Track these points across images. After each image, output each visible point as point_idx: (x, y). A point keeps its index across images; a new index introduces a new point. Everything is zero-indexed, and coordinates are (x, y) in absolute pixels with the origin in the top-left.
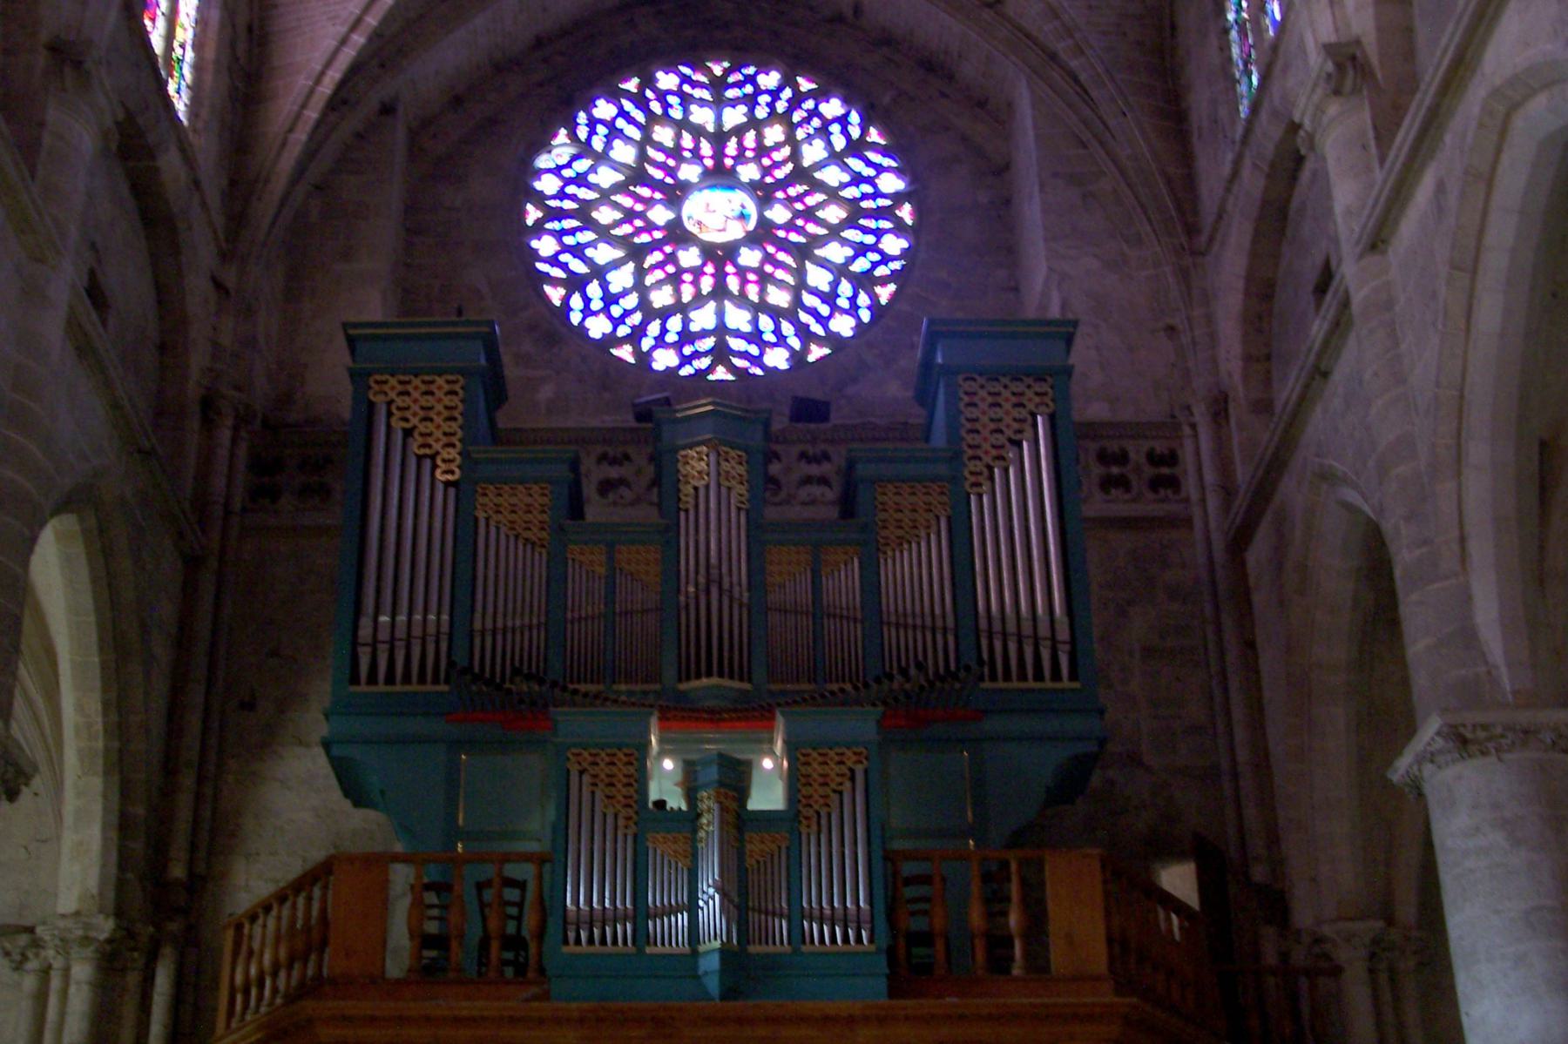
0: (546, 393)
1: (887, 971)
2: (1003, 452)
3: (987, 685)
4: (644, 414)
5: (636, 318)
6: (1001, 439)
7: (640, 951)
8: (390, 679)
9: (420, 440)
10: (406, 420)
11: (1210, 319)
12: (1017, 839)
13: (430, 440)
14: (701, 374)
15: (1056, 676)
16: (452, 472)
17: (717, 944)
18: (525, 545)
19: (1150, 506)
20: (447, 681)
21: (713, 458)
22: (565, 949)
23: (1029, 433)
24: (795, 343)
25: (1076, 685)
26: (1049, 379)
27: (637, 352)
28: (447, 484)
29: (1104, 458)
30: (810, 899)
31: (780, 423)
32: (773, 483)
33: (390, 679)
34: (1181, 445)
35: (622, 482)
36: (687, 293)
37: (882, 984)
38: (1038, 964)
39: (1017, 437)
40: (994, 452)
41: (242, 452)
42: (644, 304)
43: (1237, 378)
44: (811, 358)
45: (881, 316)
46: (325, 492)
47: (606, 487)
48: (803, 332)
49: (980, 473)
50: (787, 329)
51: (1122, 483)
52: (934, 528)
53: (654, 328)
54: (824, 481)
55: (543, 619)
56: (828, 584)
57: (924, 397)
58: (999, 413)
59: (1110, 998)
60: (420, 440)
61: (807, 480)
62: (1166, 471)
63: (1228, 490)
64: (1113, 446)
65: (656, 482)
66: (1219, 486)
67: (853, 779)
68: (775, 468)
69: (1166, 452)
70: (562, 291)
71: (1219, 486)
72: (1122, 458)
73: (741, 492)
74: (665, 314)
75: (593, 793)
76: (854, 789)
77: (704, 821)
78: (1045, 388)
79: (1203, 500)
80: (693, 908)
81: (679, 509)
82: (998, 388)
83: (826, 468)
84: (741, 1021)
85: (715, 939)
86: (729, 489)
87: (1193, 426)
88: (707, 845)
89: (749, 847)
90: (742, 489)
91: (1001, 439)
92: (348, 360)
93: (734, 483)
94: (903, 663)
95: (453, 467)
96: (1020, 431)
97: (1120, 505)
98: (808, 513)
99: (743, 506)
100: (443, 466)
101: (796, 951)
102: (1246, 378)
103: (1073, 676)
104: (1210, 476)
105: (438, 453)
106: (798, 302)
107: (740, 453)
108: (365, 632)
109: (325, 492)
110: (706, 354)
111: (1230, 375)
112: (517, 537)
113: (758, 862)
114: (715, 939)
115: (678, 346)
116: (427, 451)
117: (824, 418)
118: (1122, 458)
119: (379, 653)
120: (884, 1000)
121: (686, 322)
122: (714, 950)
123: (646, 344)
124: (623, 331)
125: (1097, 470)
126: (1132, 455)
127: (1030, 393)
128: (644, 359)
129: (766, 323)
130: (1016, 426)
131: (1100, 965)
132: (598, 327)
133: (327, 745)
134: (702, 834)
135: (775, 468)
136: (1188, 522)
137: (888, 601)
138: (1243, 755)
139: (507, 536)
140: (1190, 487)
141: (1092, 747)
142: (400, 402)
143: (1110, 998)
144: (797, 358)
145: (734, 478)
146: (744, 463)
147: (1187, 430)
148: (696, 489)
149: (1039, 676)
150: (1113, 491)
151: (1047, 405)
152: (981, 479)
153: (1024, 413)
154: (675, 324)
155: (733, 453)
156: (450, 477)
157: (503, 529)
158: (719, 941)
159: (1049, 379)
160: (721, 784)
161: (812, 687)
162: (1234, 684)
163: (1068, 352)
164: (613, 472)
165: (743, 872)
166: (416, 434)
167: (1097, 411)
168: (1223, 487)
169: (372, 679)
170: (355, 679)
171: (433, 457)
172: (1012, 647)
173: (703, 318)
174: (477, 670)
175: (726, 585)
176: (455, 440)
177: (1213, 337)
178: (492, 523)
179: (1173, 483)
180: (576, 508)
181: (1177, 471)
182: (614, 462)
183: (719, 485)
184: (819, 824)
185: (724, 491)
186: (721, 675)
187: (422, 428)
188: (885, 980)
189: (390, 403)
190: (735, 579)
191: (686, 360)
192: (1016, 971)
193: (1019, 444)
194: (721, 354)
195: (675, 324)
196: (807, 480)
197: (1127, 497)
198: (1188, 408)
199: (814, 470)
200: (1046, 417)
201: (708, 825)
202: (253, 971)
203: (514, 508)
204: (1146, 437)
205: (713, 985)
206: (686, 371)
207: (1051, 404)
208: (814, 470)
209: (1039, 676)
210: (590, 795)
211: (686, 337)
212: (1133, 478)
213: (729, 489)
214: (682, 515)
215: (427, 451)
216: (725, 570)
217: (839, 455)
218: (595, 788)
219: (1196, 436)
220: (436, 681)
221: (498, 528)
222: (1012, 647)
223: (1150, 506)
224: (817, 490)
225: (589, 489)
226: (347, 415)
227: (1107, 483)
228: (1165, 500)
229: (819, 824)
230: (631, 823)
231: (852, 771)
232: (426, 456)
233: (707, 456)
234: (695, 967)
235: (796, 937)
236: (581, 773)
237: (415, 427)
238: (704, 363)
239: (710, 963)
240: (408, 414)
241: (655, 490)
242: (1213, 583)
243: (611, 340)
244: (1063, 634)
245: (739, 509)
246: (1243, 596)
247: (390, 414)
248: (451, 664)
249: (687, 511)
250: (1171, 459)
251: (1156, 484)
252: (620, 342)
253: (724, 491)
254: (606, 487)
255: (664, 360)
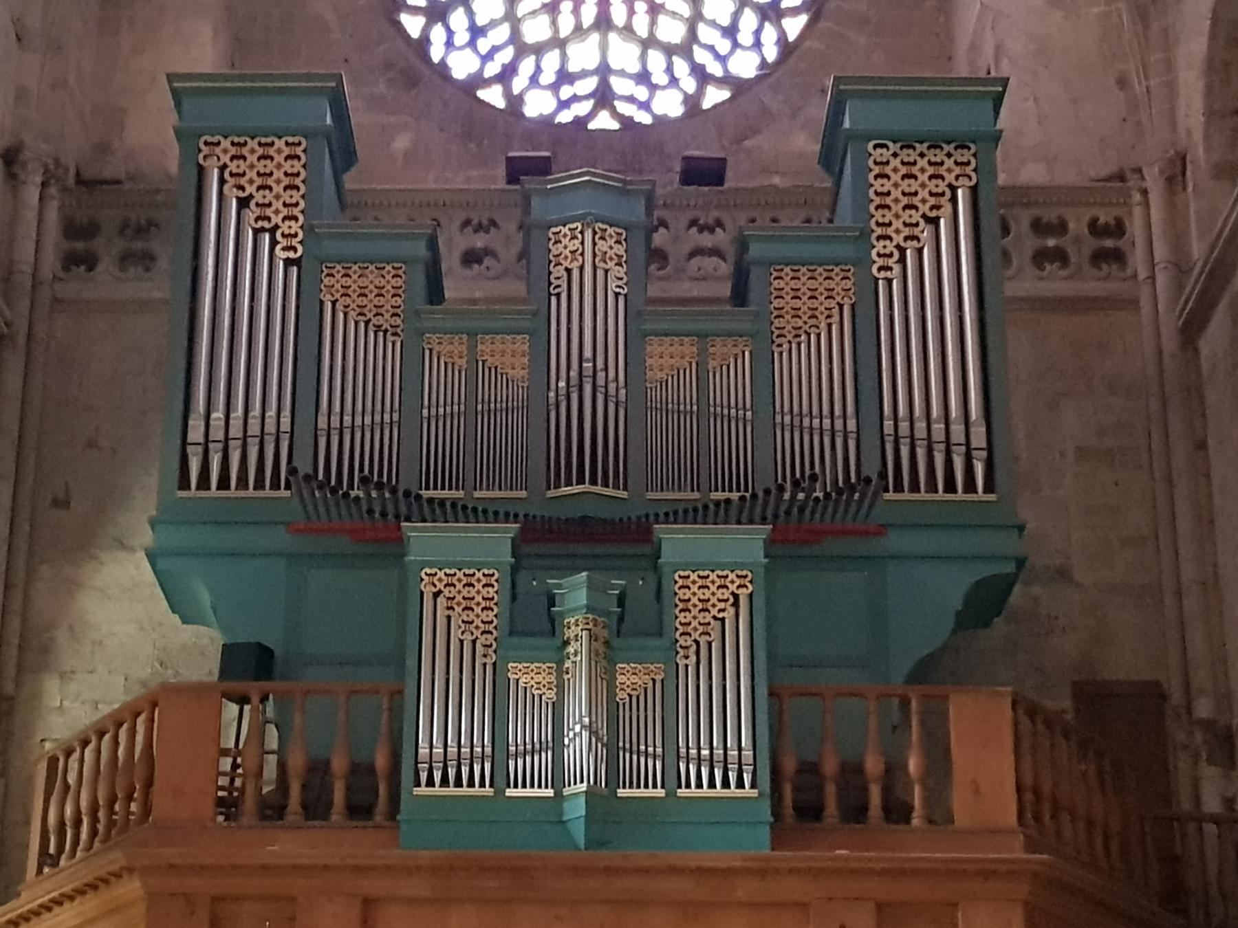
0: (401, 143)
1: (772, 819)
2: (916, 231)
3: (890, 496)
4: (517, 170)
5: (506, 55)
6: (916, 217)
7: (500, 793)
8: (224, 483)
9: (258, 212)
10: (242, 188)
11: (1169, 65)
12: (920, 674)
13: (269, 212)
14: (580, 122)
15: (970, 486)
16: (295, 250)
17: (583, 787)
18: (376, 333)
19: (1091, 285)
20: (288, 487)
21: (588, 234)
22: (417, 791)
23: (948, 208)
24: (689, 85)
25: (992, 497)
26: (972, 146)
27: (508, 93)
28: (288, 262)
29: (1038, 227)
30: (687, 736)
31: (668, 184)
32: (658, 256)
33: (224, 483)
34: (1130, 213)
35: (488, 252)
36: (566, 24)
37: (765, 833)
38: (940, 816)
39: (934, 214)
40: (906, 231)
41: (53, 216)
42: (515, 38)
43: (1198, 136)
44: (707, 104)
45: (791, 53)
46: (148, 259)
47: (471, 258)
48: (700, 73)
49: (891, 255)
50: (681, 67)
51: (1060, 256)
52: (836, 318)
53: (527, 66)
54: (716, 252)
55: (396, 417)
56: (716, 383)
57: (830, 158)
58: (914, 186)
59: (1020, 854)
60: (258, 212)
61: (697, 252)
62: (1109, 243)
63: (1180, 268)
64: (1050, 215)
65: (523, 255)
66: (1169, 262)
67: (736, 604)
68: (659, 238)
69: (1113, 223)
70: (421, 21)
71: (1169, 262)
72: (1060, 228)
73: (619, 275)
74: (539, 50)
75: (449, 618)
76: (737, 615)
77: (571, 649)
78: (965, 156)
79: (1152, 277)
80: (557, 745)
81: (550, 294)
82: (912, 156)
83: (720, 238)
84: (609, 871)
85: (582, 781)
86: (606, 271)
87: (1145, 192)
88: (574, 676)
89: (620, 679)
90: (621, 272)
91: (916, 217)
92: (173, 117)
93: (611, 264)
94: (798, 475)
95: (295, 242)
96: (936, 207)
97: (1054, 283)
98: (697, 290)
99: (621, 291)
100: (284, 242)
101: (671, 794)
102: (1207, 137)
103: (989, 488)
104: (1161, 252)
105: (277, 227)
106: (692, 36)
107: (620, 231)
108: (196, 433)
109: (148, 259)
110: (587, 97)
111: (1189, 133)
112: (367, 323)
113: (630, 696)
114: (582, 781)
115: (555, 87)
116: (266, 225)
117: (720, 181)
118: (1060, 228)
119: (211, 453)
120: (767, 851)
121: (564, 58)
122: (582, 792)
123: (518, 84)
124: (492, 69)
125: (1031, 243)
126: (1072, 226)
127: (949, 163)
128: (515, 102)
129: (656, 61)
130: (932, 201)
131: (1010, 818)
132: (462, 66)
133: (152, 557)
134: (568, 664)
135: (659, 238)
136: (1134, 303)
137: (783, 401)
138: (1188, 573)
139: (356, 323)
140: (1138, 259)
141: (1010, 568)
142: (233, 167)
143: (1020, 854)
144: (692, 103)
145: (611, 259)
146: (623, 242)
147: (1137, 197)
148: (568, 271)
149: (950, 487)
150: (1048, 267)
151: (970, 178)
152: (891, 262)
153: (942, 187)
154: (551, 62)
155: (610, 231)
156: (291, 255)
157: (352, 314)
158: (585, 784)
159: (972, 146)
160: (589, 609)
161: (696, 495)
162: (1181, 490)
163: (997, 112)
164: (480, 241)
165: (614, 708)
166: (252, 204)
167: (1034, 174)
168: (1176, 265)
169: (204, 483)
170: (184, 484)
171: (273, 231)
172: (921, 452)
173: (583, 55)
174: (321, 477)
175: (601, 381)
176: (296, 211)
177: (1171, 87)
178: (339, 306)
179: (1117, 257)
180: (435, 293)
181: (1122, 243)
182: (479, 228)
183: (595, 268)
184: (698, 653)
185: (600, 273)
186: (593, 482)
187: (259, 197)
188: (768, 828)
189: (223, 168)
190: (612, 374)
191: (564, 105)
192: (915, 822)
193: (934, 222)
194: (604, 97)
195: (551, 62)
196: (697, 252)
197: (1064, 273)
198: (1139, 171)
199: (707, 240)
200: (967, 191)
201: (576, 654)
202: (69, 811)
203: (379, 310)
204: (1088, 204)
205: (579, 833)
206: (565, 117)
207: (973, 175)
208: (707, 240)
209: (950, 487)
210: (445, 621)
211: (565, 77)
212: (1071, 250)
213: (606, 271)
214: (554, 300)
215: (266, 225)
216: (600, 364)
217: (736, 221)
218: (450, 612)
219: (1146, 204)
220: (275, 485)
221: (346, 314)
222: (921, 452)
223: (1091, 285)
224: (710, 262)
225: (450, 261)
226: (173, 167)
227: (1041, 257)
228: (1107, 277)
229: (698, 653)
230: (490, 651)
231: (736, 596)
232: (263, 230)
233: (582, 232)
234: (561, 813)
235: (671, 778)
236: (436, 595)
237: (251, 196)
238: (582, 109)
239: (576, 810)
240: (243, 181)
241: (524, 261)
242: (1161, 371)
243: (478, 80)
244: (979, 438)
245: (617, 295)
246: (1194, 392)
247: (222, 181)
248: (292, 471)
249: (558, 295)
250: (1119, 229)
251: (1099, 257)
252: (487, 83)
253: (600, 273)
254: (471, 258)
255: (538, 105)
